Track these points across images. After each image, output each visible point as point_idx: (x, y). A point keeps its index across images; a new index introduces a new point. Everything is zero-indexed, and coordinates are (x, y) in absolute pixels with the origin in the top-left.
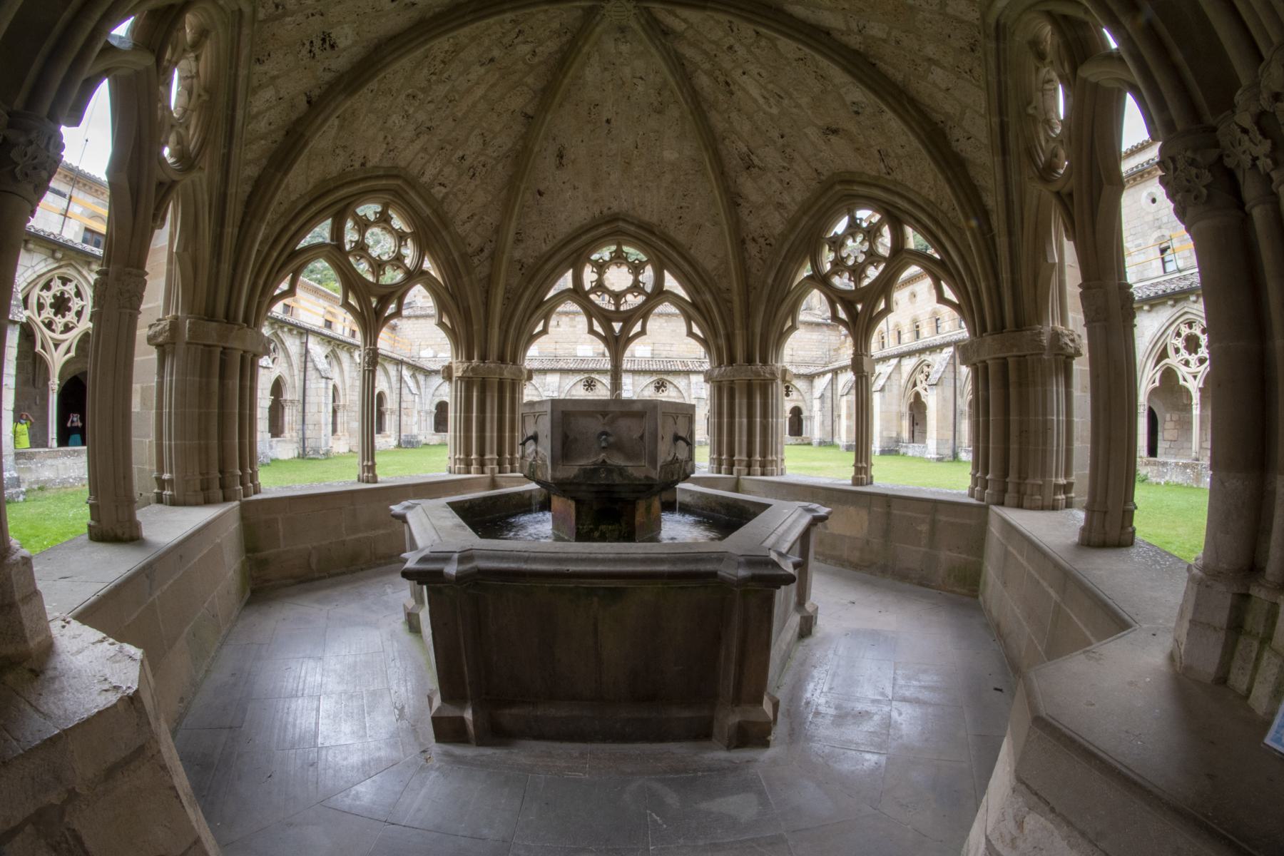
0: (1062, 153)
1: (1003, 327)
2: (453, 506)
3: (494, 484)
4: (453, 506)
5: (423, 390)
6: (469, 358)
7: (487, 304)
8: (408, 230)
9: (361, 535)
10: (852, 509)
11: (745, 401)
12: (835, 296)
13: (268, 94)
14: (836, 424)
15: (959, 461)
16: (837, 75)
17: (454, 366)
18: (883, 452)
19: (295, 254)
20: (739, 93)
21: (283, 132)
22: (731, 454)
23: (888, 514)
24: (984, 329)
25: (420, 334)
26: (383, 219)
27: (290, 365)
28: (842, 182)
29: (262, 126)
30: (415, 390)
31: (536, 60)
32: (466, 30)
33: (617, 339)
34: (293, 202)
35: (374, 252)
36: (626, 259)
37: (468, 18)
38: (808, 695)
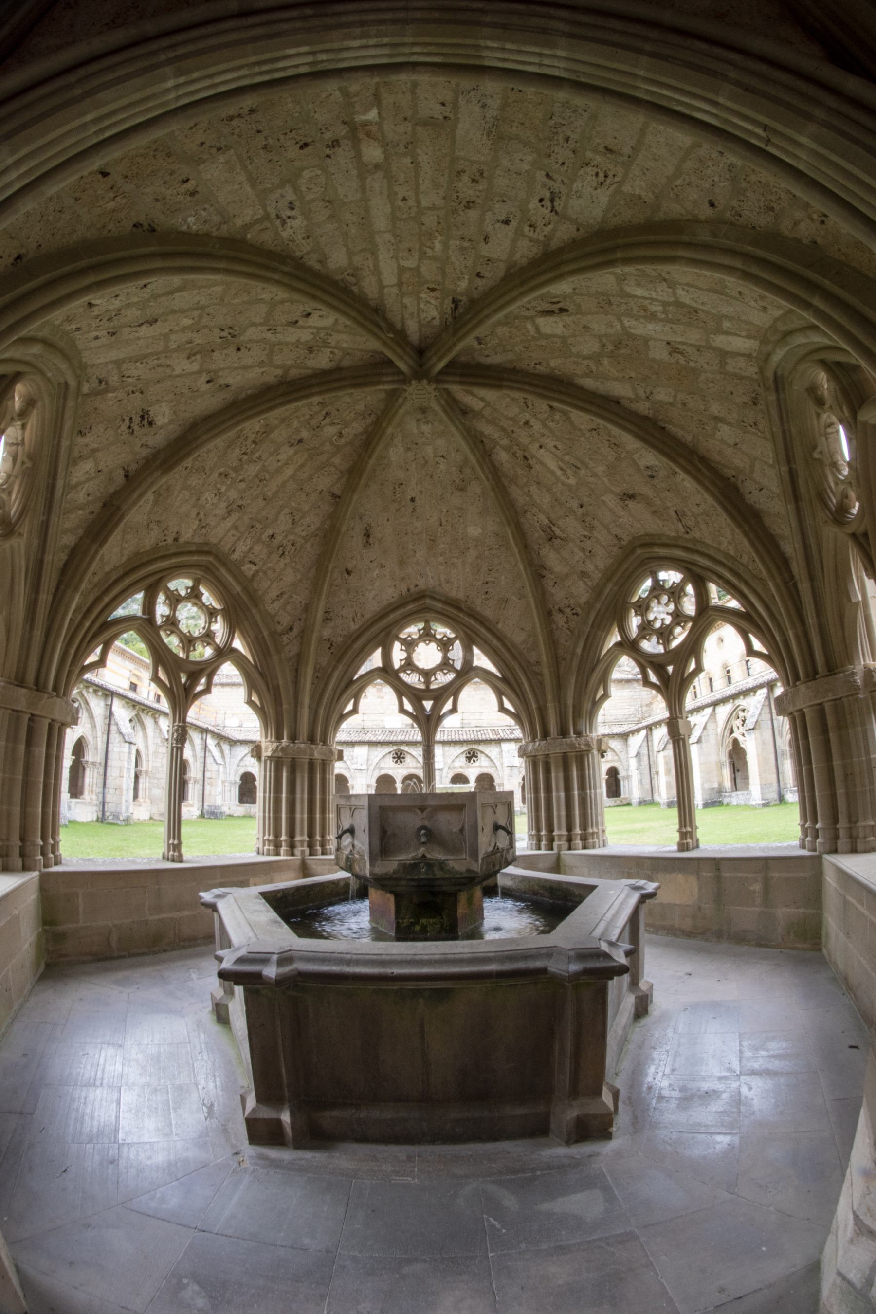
0: (852, 494)
1: (816, 673)
2: (265, 895)
3: (305, 870)
4: (265, 895)
5: (227, 760)
6: (279, 737)
7: (296, 682)
8: (218, 607)
9: (164, 916)
10: (680, 877)
11: (561, 775)
12: (645, 661)
13: (88, 466)
14: (655, 781)
15: (786, 803)
16: (630, 442)
17: (263, 745)
18: (706, 805)
19: (106, 626)
20: (537, 467)
21: (101, 504)
22: (550, 830)
23: (718, 879)
24: (797, 678)
25: (229, 705)
26: (194, 595)
27: (94, 726)
28: (643, 545)
29: (80, 496)
30: (219, 760)
31: (343, 441)
32: (277, 412)
33: (428, 718)
34: (107, 574)
35: (183, 627)
36: (434, 636)
37: (278, 401)
38: (650, 1079)
